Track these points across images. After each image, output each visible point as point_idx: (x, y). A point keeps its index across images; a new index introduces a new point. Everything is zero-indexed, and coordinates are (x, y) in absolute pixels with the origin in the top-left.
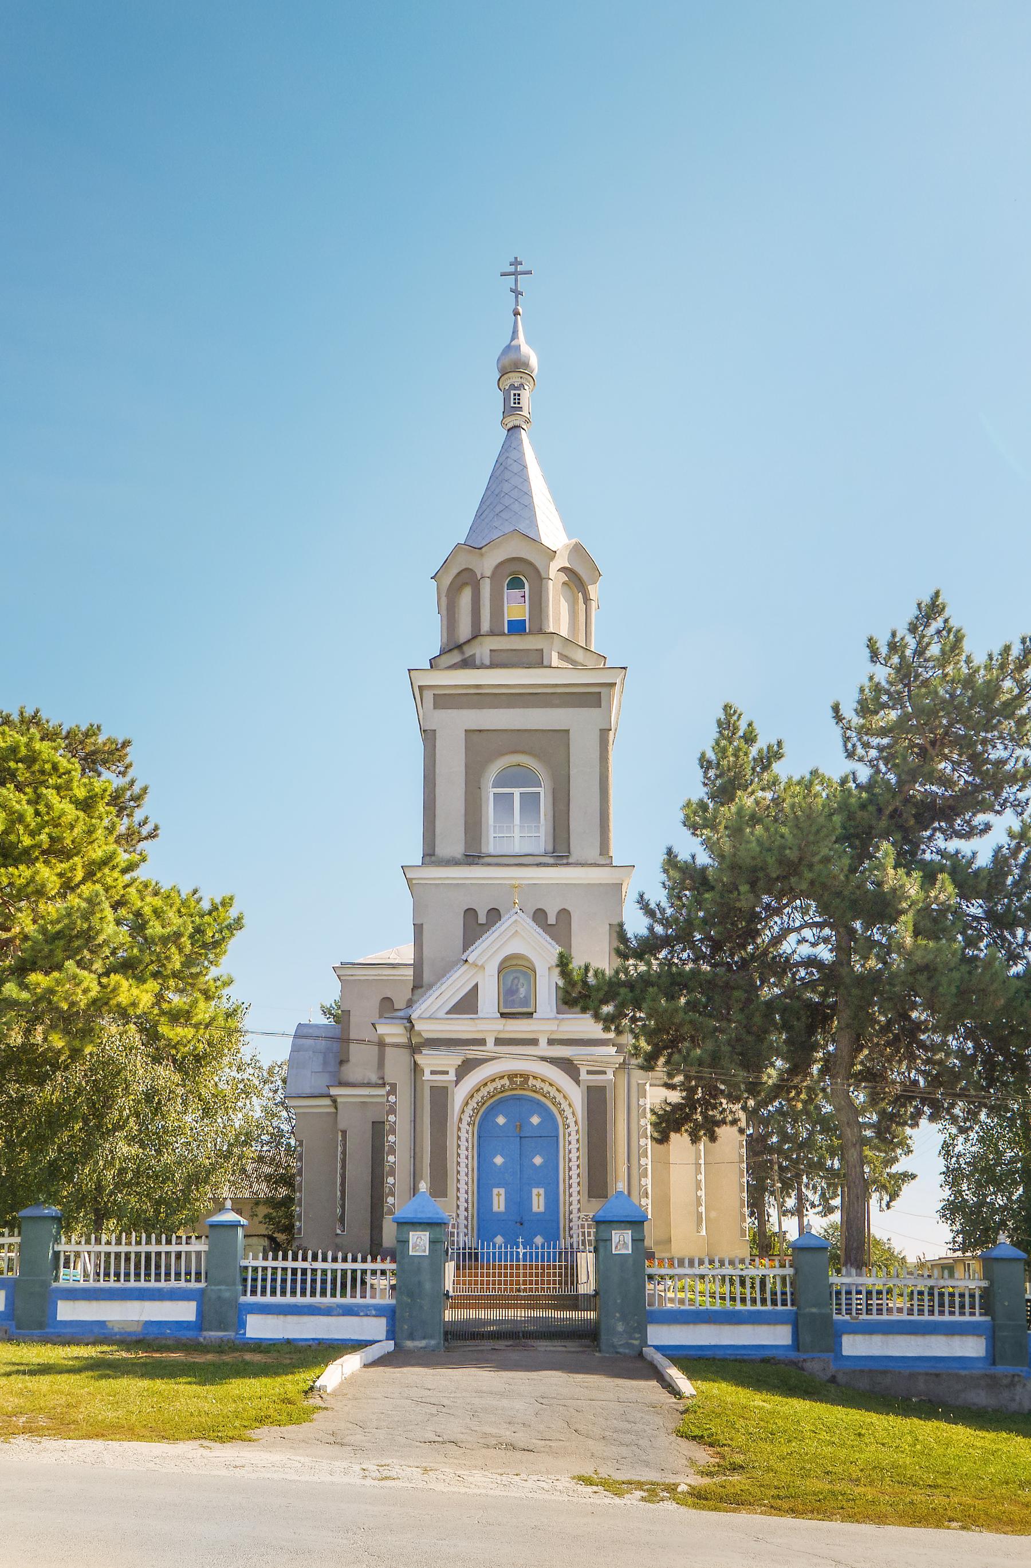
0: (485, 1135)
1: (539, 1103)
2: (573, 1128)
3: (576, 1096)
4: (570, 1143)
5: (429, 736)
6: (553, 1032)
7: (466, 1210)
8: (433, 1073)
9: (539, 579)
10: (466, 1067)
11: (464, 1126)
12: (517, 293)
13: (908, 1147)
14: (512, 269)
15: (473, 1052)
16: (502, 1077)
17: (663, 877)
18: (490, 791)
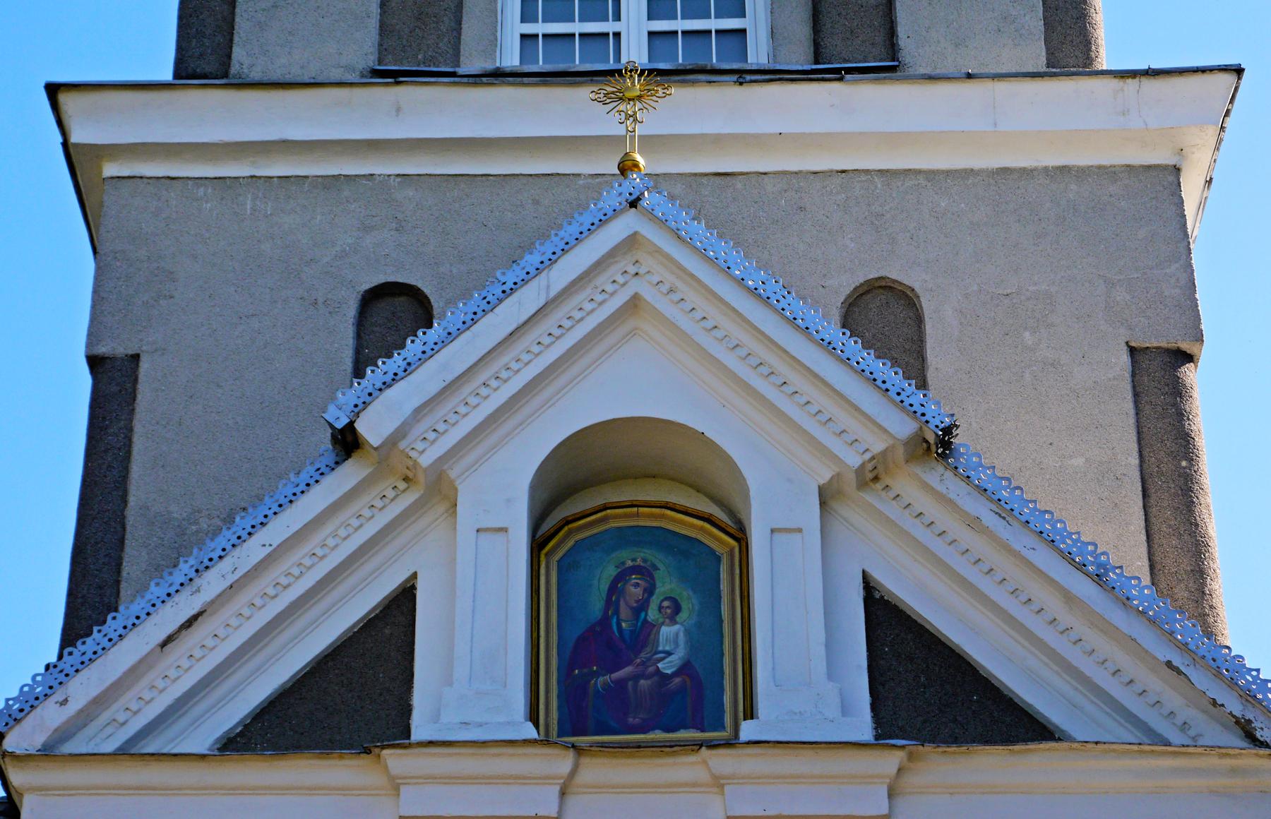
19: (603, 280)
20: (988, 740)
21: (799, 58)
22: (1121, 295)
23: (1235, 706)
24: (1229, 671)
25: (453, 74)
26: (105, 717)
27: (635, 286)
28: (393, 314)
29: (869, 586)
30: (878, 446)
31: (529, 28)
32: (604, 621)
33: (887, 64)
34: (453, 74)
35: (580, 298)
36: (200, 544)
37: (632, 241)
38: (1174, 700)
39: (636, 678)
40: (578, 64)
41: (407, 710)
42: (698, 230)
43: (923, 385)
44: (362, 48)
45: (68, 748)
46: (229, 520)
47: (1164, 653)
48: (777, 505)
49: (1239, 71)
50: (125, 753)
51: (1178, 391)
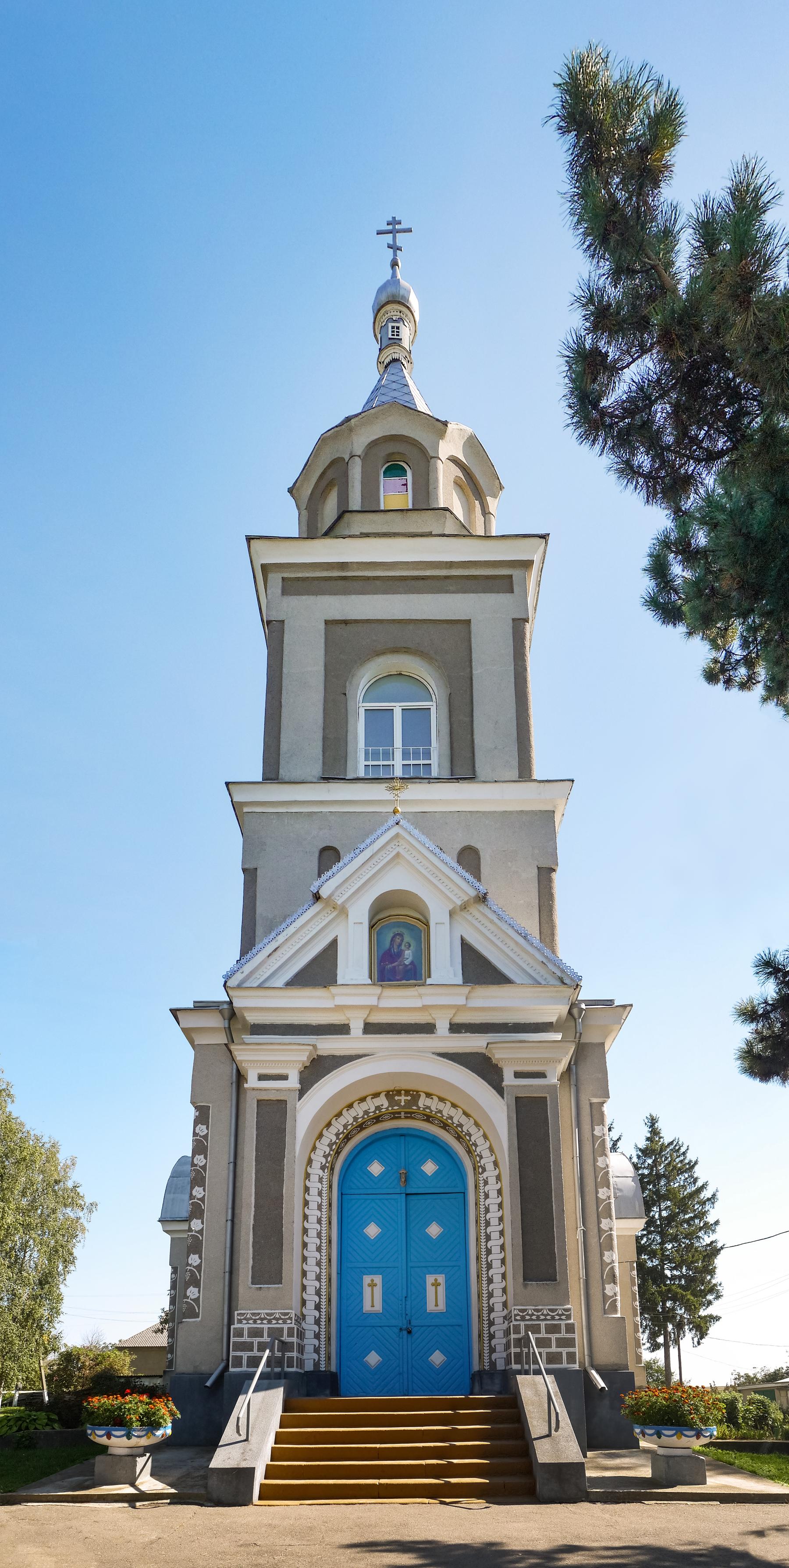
0: (349, 1192)
1: (434, 1141)
2: (491, 1173)
3: (497, 1113)
4: (487, 1196)
5: (274, 631)
6: (459, 1008)
7: (318, 1307)
8: (262, 1077)
9: (425, 460)
10: (316, 1069)
11: (316, 1170)
12: (394, 248)
13: (718, 1291)
14: (390, 227)
15: (329, 1045)
16: (376, 1095)
17: (682, 629)
18: (360, 707)
19: (389, 847)
20: (493, 984)
21: (446, 774)
22: (537, 851)
23: (559, 974)
24: (558, 964)
25: (344, 779)
26: (254, 976)
27: (398, 849)
28: (329, 856)
29: (462, 939)
30: (466, 899)
31: (367, 763)
32: (390, 949)
33: (471, 777)
34: (344, 779)
35: (382, 853)
36: (277, 926)
37: (397, 835)
38: (543, 972)
39: (398, 966)
40: (382, 776)
41: (336, 975)
42: (416, 832)
43: (479, 880)
44: (316, 769)
45: (245, 985)
46: (285, 919)
47: (541, 959)
48: (438, 915)
49: (573, 781)
50: (260, 987)
51: (550, 880)
